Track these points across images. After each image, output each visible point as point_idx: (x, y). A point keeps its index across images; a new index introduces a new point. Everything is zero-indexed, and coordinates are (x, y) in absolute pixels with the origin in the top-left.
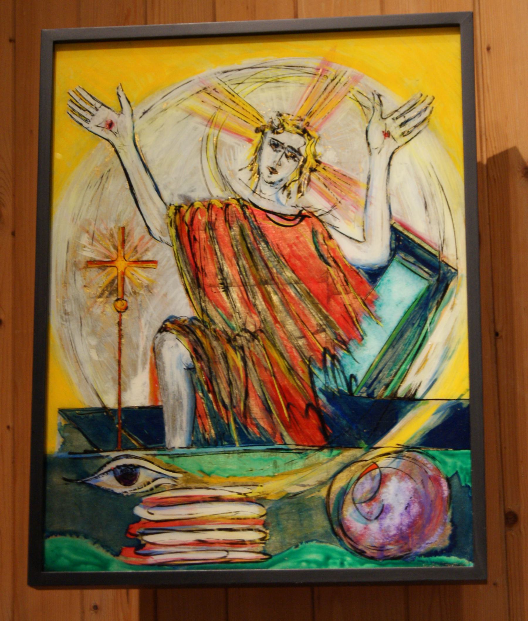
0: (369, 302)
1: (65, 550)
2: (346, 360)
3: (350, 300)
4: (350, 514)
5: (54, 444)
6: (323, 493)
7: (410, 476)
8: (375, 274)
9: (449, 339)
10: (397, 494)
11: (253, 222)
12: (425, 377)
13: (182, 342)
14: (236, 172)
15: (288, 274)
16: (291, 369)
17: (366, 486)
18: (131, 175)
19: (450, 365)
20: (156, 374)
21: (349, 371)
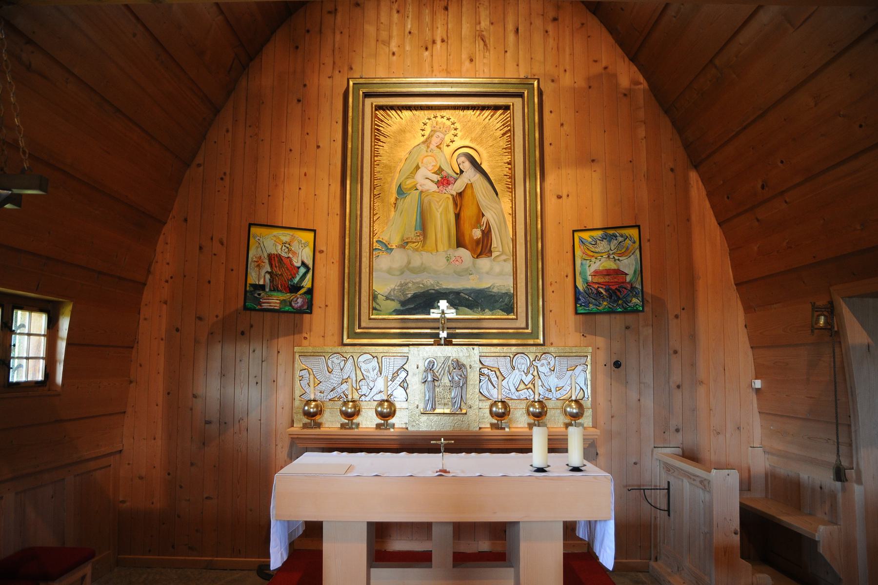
0: (298, 272)
1: (249, 304)
5: (248, 289)
8: (299, 268)
10: (300, 300)
14: (279, 250)
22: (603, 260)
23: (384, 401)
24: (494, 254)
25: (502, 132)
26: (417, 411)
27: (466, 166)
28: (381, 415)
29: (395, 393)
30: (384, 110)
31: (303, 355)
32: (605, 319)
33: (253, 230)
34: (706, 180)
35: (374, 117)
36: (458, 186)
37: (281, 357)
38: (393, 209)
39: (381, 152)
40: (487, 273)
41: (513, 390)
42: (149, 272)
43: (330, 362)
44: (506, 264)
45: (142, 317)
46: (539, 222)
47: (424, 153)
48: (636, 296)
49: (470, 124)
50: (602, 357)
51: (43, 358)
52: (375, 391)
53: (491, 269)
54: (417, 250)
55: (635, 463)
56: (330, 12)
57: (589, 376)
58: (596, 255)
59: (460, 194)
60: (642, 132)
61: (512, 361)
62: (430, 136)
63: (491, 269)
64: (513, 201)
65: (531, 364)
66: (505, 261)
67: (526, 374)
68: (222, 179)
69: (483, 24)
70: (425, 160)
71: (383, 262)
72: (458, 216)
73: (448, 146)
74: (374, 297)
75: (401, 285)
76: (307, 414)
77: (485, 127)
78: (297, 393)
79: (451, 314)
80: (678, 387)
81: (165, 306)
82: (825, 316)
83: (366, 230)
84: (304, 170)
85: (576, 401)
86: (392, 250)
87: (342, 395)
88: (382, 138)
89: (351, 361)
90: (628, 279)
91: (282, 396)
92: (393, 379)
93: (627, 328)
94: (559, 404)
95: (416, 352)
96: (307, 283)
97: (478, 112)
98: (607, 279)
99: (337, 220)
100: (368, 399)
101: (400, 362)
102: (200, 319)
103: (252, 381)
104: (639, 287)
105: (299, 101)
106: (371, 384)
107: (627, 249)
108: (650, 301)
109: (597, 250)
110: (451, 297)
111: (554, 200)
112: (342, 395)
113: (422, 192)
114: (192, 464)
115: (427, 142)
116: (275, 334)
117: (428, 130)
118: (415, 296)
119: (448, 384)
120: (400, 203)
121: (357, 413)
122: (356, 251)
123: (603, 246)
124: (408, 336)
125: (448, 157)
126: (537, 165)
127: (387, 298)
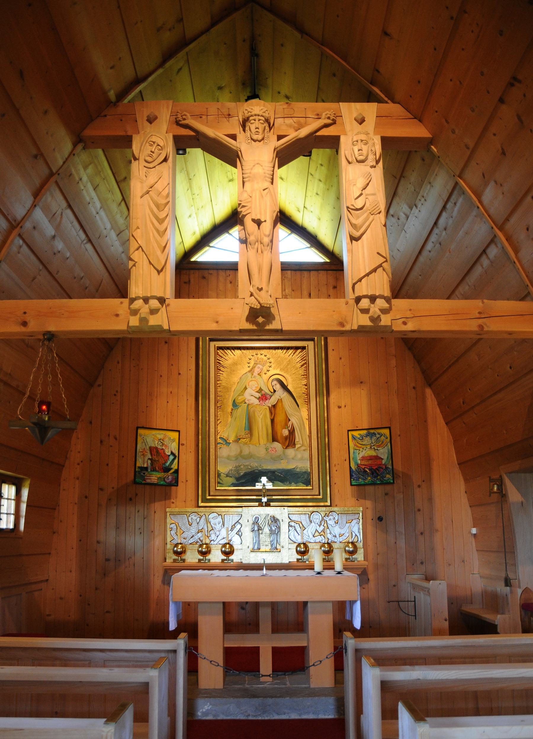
0: (168, 458)
1: (138, 480)
8: (169, 456)
10: (170, 477)
11: (171, 529)
18: (145, 442)
20: (147, 464)
22: (367, 449)
23: (226, 544)
24: (297, 446)
25: (301, 364)
26: (249, 550)
27: (278, 387)
28: (225, 553)
29: (233, 539)
30: (223, 350)
31: (172, 514)
32: (370, 489)
33: (140, 431)
34: (437, 395)
35: (216, 354)
36: (273, 401)
37: (157, 515)
38: (230, 416)
39: (221, 378)
40: (293, 459)
41: (311, 536)
42: (66, 458)
43: (190, 518)
45: (61, 487)
46: (326, 424)
47: (250, 378)
48: (389, 474)
49: (279, 359)
50: (370, 514)
51: (13, 514)
52: (220, 537)
53: (295, 456)
54: (246, 444)
55: (394, 586)
56: (185, 283)
57: (361, 527)
58: (363, 446)
59: (274, 406)
60: (393, 362)
61: (309, 517)
62: (254, 367)
63: (295, 456)
64: (309, 410)
65: (323, 519)
67: (320, 526)
68: (115, 395)
69: (287, 291)
70: (250, 383)
71: (224, 451)
72: (273, 421)
73: (265, 374)
75: (236, 467)
76: (176, 553)
77: (289, 361)
78: (169, 540)
79: (269, 486)
80: (422, 534)
81: (77, 481)
82: (497, 485)
83: (212, 430)
84: (170, 390)
85: (352, 543)
86: (230, 443)
87: (198, 540)
88: (222, 368)
89: (204, 517)
90: (383, 462)
91: (157, 542)
92: (232, 530)
93: (386, 494)
94: (342, 545)
95: (247, 511)
96: (175, 466)
97: (285, 351)
98: (370, 462)
99: (193, 423)
100: (215, 543)
101: (236, 518)
102: (102, 489)
103: (137, 532)
104: (390, 467)
105: (166, 342)
106: (218, 533)
107: (383, 443)
108: (401, 476)
109: (363, 443)
110: (269, 474)
111: (336, 409)
112: (198, 540)
113: (248, 405)
114: (96, 589)
115: (251, 371)
116: (153, 500)
117: (252, 363)
118: (246, 474)
119: (268, 532)
120: (234, 412)
121: (208, 552)
122: (206, 445)
123: (367, 441)
124: (241, 500)
125: (266, 381)
126: (324, 387)
127: (227, 476)
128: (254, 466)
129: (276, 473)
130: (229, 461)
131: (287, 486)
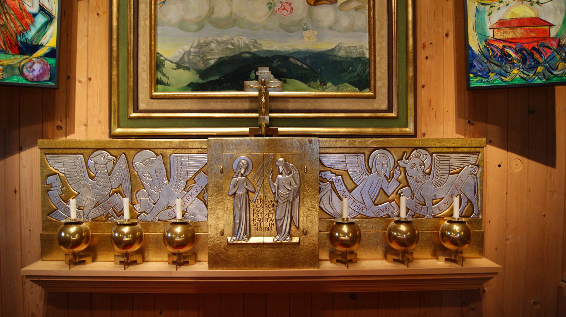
0: (33, 22)
2: (26, 35)
3: (28, 21)
4: (25, 70)
6: (18, 65)
7: (40, 63)
8: (35, 15)
9: (52, 33)
12: (46, 41)
13: (365, 257)
15: (12, 12)
16: (12, 35)
17: (30, 64)
19: (52, 39)
21: (27, 37)
40: (331, 28)
43: (91, 162)
44: (359, 14)
63: (336, 21)
66: (357, 9)
74: (157, 64)
75: (200, 46)
90: (553, 32)
98: (519, 33)
110: (275, 64)
118: (221, 63)
127: (179, 65)
128: (241, 43)
129: (292, 60)
130: (182, 33)
131: (317, 89)
